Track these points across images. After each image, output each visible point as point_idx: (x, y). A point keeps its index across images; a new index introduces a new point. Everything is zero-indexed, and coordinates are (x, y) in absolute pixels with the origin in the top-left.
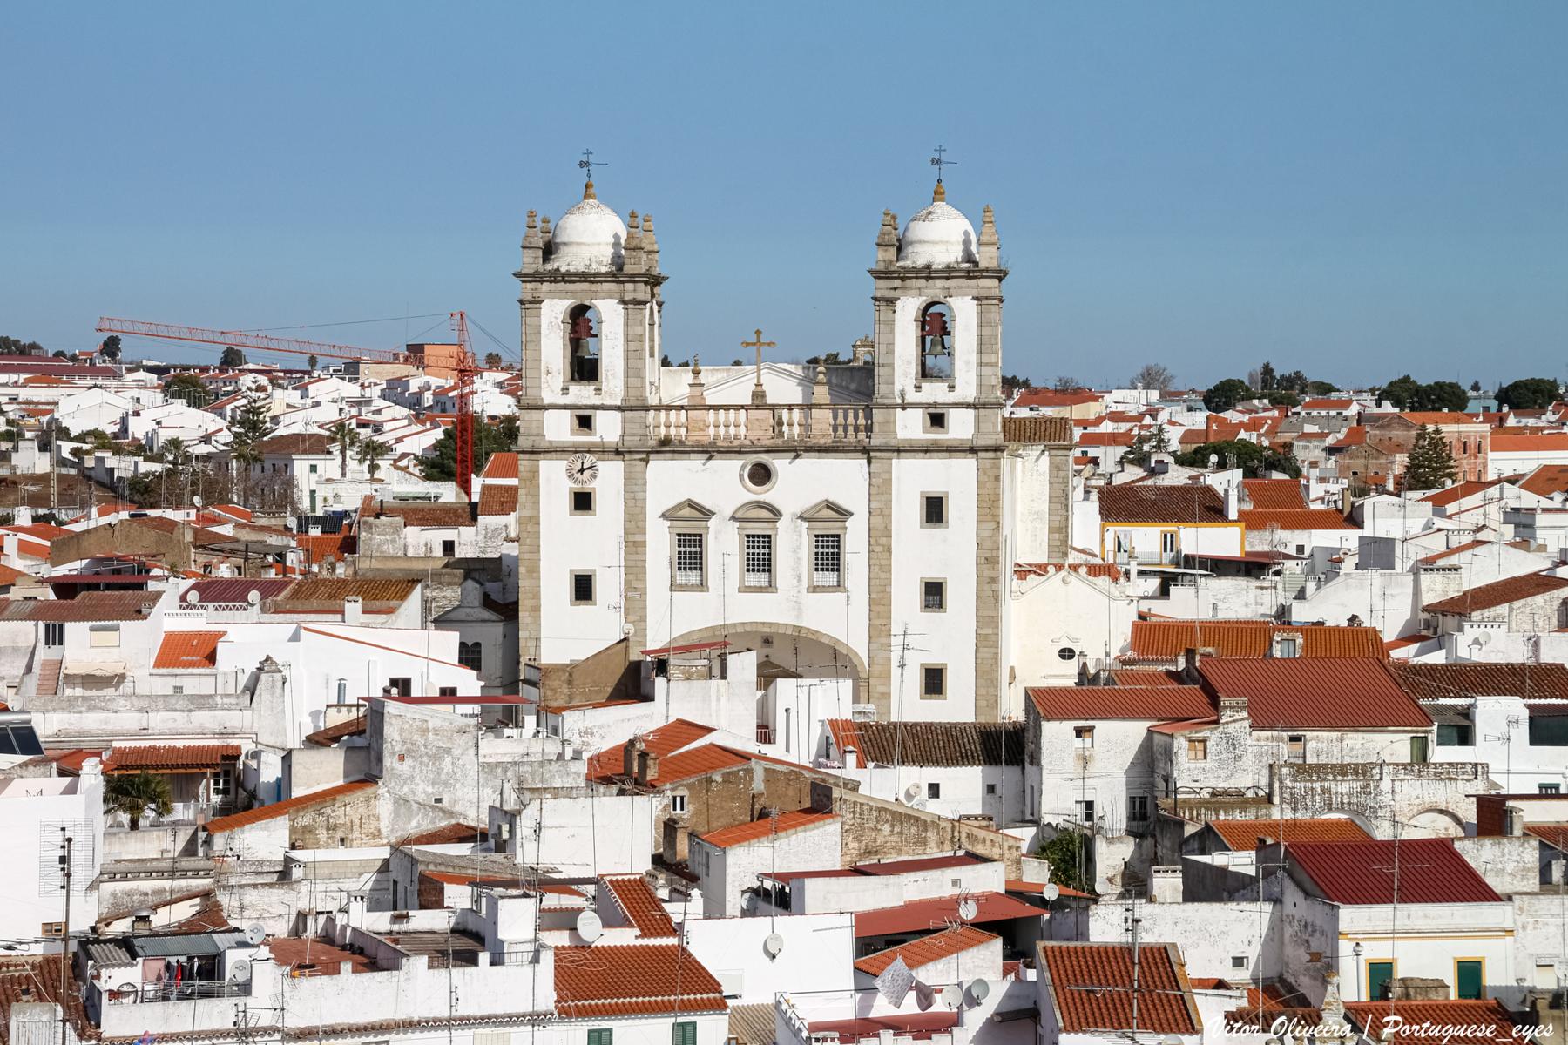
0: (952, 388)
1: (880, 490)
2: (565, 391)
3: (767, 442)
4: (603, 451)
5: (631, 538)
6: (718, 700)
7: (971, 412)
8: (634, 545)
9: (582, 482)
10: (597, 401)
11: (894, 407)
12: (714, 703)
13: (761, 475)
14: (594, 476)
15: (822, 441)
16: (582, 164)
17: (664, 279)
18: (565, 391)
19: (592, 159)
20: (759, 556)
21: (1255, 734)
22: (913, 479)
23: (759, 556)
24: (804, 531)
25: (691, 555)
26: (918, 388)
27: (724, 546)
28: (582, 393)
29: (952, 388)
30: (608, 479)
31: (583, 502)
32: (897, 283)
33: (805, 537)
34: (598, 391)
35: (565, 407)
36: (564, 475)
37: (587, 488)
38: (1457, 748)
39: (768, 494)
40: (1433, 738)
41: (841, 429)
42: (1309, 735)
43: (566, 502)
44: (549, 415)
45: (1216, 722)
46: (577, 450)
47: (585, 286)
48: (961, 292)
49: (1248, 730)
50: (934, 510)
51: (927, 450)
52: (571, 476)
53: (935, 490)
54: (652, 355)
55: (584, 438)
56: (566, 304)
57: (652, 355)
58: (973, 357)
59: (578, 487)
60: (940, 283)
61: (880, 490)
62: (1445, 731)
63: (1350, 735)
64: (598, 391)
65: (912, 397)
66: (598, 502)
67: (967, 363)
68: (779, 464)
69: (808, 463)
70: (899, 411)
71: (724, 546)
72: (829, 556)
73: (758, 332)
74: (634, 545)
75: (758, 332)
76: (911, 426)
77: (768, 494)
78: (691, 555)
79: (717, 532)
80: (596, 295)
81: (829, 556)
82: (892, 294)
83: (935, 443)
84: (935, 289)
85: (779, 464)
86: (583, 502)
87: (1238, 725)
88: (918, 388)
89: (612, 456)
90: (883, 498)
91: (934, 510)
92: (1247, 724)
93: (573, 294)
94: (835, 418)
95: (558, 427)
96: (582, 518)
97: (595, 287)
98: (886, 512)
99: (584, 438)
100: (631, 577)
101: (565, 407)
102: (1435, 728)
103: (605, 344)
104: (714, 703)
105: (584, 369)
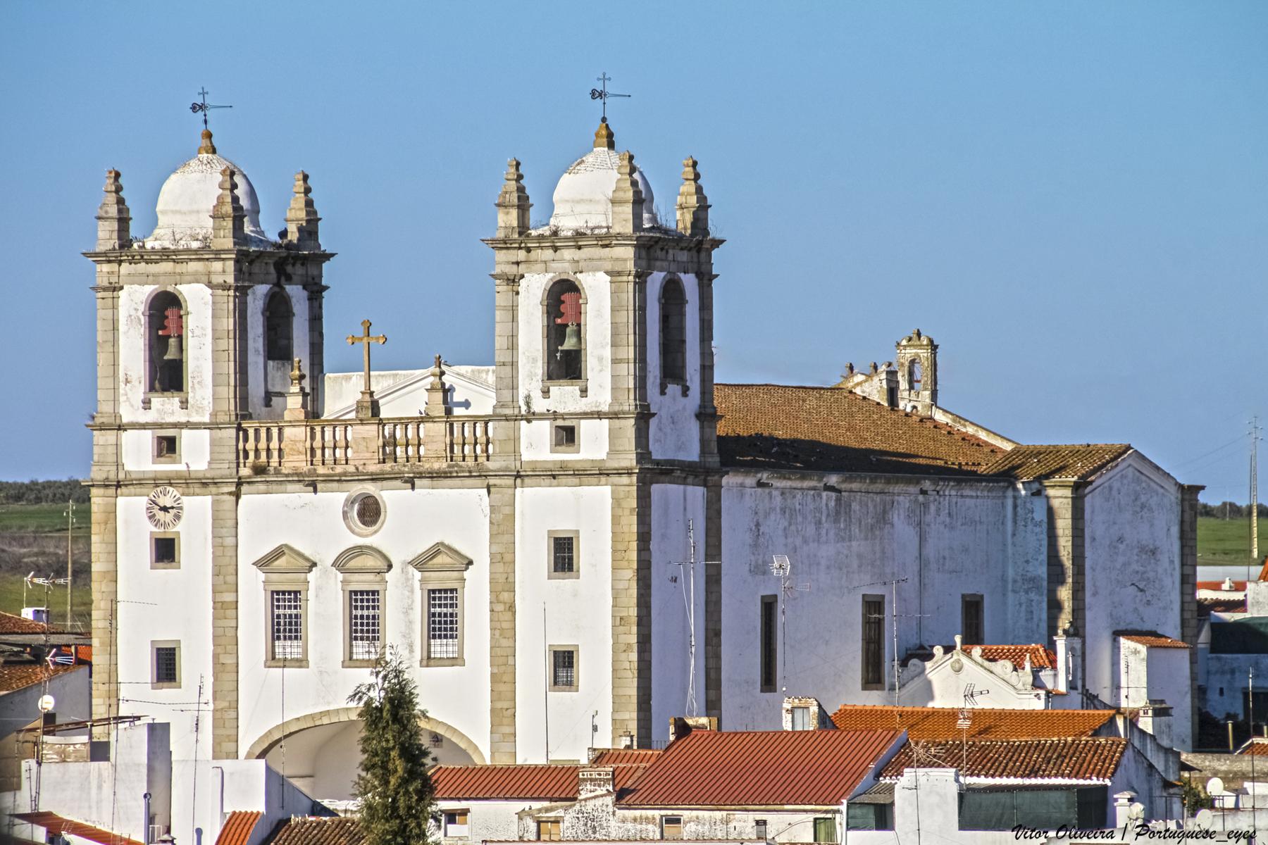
0: (584, 392)
2: (147, 404)
3: (373, 468)
5: (220, 598)
6: (100, 787)
7: (606, 423)
8: (225, 609)
9: (165, 525)
10: (181, 417)
11: (516, 418)
12: (94, 791)
13: (370, 512)
14: (177, 517)
15: (436, 466)
16: (195, 108)
18: (147, 404)
19: (209, 101)
20: (363, 618)
21: (620, 813)
22: (541, 510)
23: (363, 618)
24: (417, 585)
25: (286, 624)
26: (546, 393)
28: (166, 407)
29: (584, 392)
31: (165, 551)
32: (522, 255)
33: (418, 593)
34: (184, 404)
35: (144, 426)
37: (169, 532)
38: (875, 833)
39: (377, 538)
40: (841, 819)
41: (263, 454)
42: (686, 815)
43: (146, 551)
44: (127, 437)
45: (575, 799)
46: (158, 482)
47: (167, 267)
49: (611, 809)
50: (564, 554)
51: (554, 474)
53: (564, 526)
55: (166, 467)
58: (607, 353)
59: (159, 532)
60: (568, 254)
62: (857, 811)
63: (739, 815)
64: (184, 404)
65: (540, 405)
66: (184, 551)
67: (600, 359)
68: (391, 497)
69: (424, 493)
70: (523, 423)
72: (442, 621)
73: (368, 326)
74: (225, 609)
75: (368, 326)
76: (536, 443)
77: (377, 538)
78: (286, 624)
79: (319, 588)
80: (181, 278)
81: (442, 621)
82: (513, 270)
84: (563, 263)
85: (391, 497)
86: (165, 551)
87: (599, 802)
88: (546, 393)
89: (548, 481)
90: (506, 538)
91: (564, 554)
92: (609, 800)
93: (155, 278)
95: (137, 454)
97: (180, 268)
98: (508, 557)
99: (166, 467)
100: (219, 650)
101: (144, 426)
102: (843, 808)
103: (191, 344)
104: (94, 791)
105: (167, 375)
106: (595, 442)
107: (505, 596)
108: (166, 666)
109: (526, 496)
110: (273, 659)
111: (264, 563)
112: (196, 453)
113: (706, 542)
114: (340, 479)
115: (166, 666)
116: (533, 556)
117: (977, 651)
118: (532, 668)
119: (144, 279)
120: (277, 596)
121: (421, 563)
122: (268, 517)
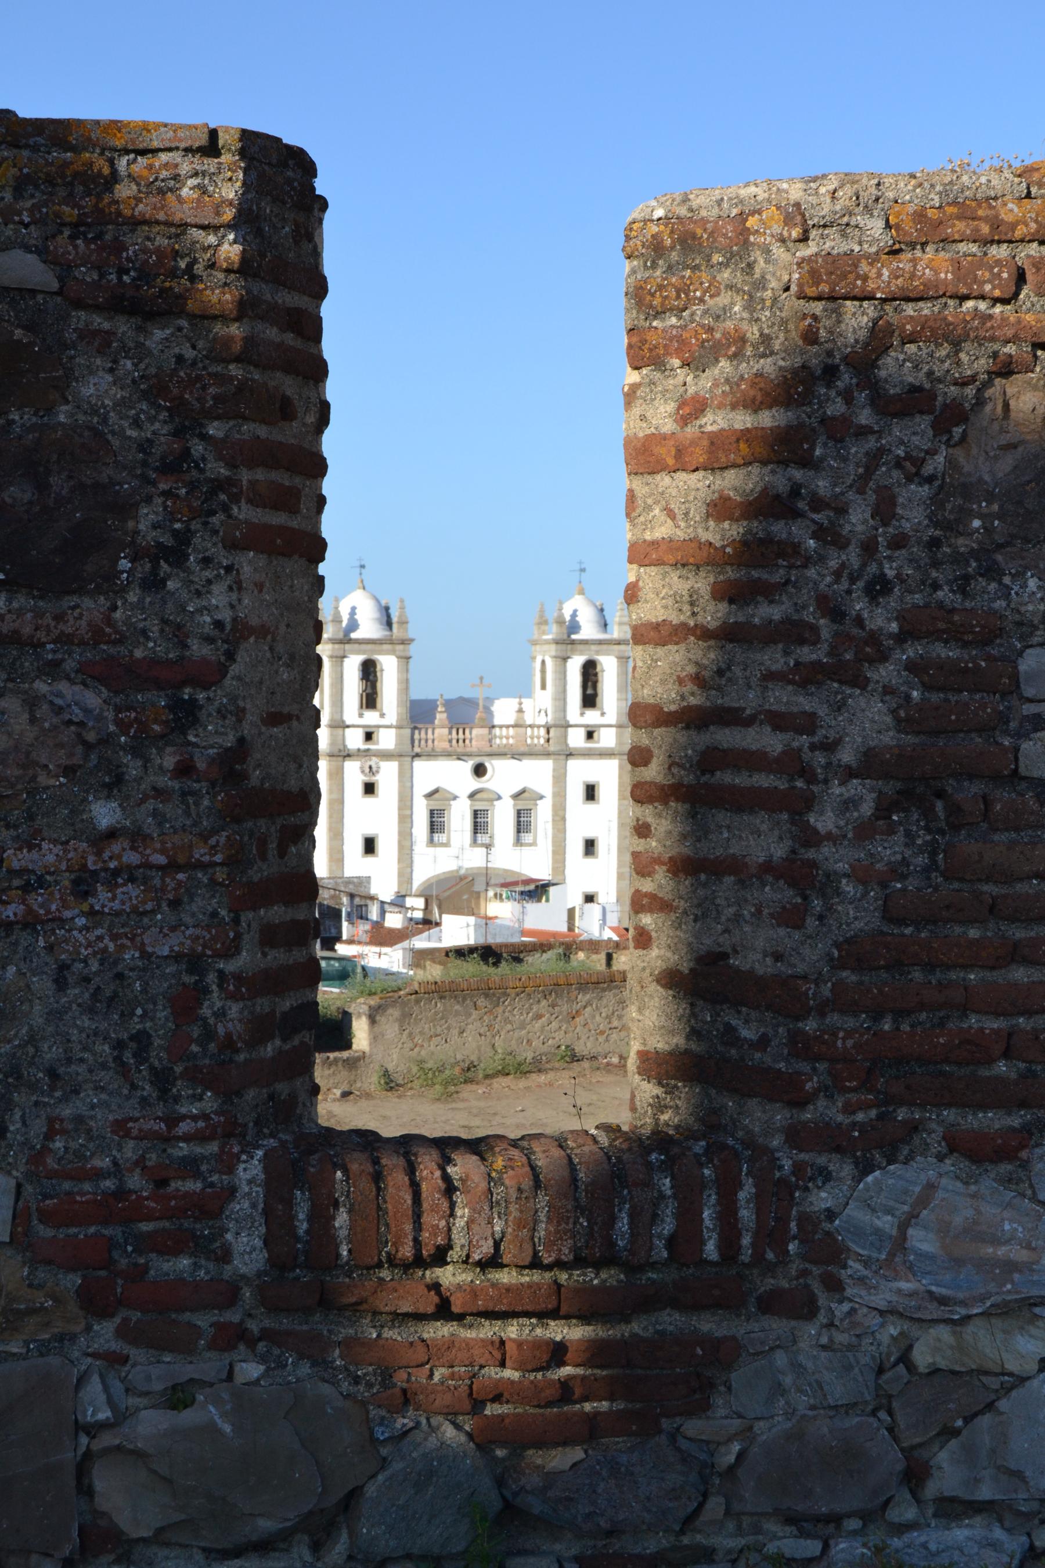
1: (560, 779)
4: (386, 755)
13: (479, 771)
17: (412, 640)
20: (479, 824)
22: (580, 772)
23: (479, 824)
25: (436, 824)
27: (459, 818)
29: (603, 714)
30: (388, 775)
31: (369, 789)
34: (382, 715)
36: (359, 771)
37: (373, 779)
41: (454, 742)
43: (360, 789)
46: (365, 754)
48: (607, 653)
50: (591, 793)
52: (363, 772)
53: (591, 779)
54: (543, 687)
55: (590, 745)
56: (361, 658)
57: (543, 687)
59: (367, 779)
61: (560, 779)
71: (459, 818)
72: (522, 824)
73: (481, 678)
74: (405, 818)
75: (481, 678)
76: (576, 739)
78: (436, 824)
83: (590, 749)
86: (369, 789)
91: (591, 793)
94: (450, 733)
96: (370, 800)
99: (590, 745)
106: (607, 739)
107: (561, 813)
108: (370, 846)
109: (572, 764)
110: (431, 842)
111: (429, 796)
112: (387, 740)
113: (400, 842)
114: (470, 755)
115: (370, 846)
116: (575, 793)
117: (519, 1059)
118: (575, 847)
119: (358, 652)
120: (432, 813)
121: (516, 796)
122: (429, 774)
